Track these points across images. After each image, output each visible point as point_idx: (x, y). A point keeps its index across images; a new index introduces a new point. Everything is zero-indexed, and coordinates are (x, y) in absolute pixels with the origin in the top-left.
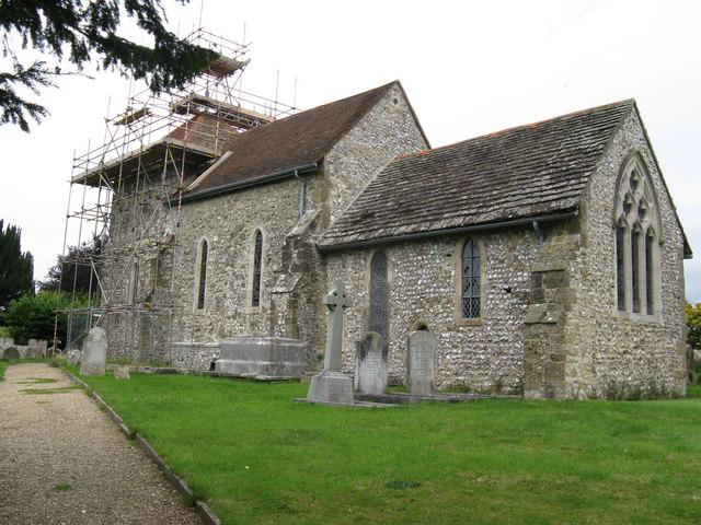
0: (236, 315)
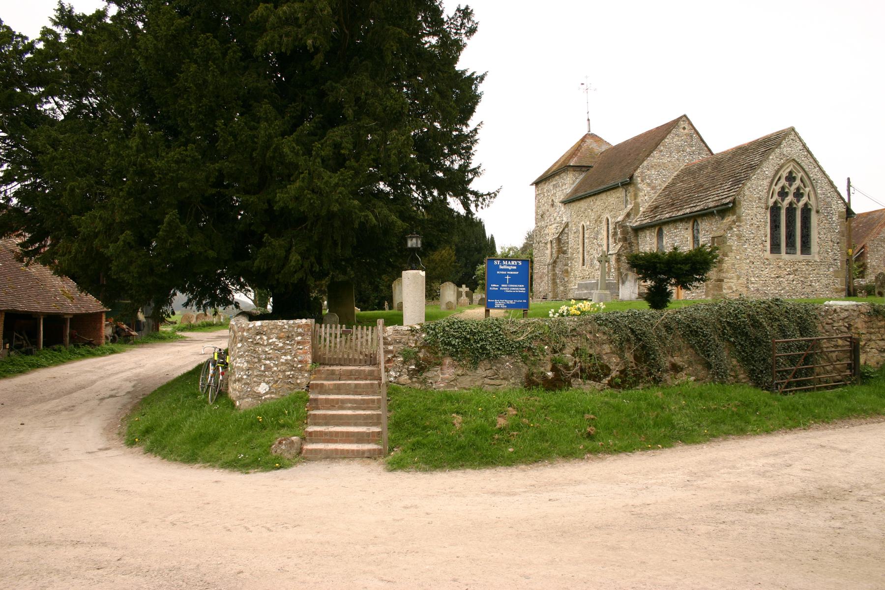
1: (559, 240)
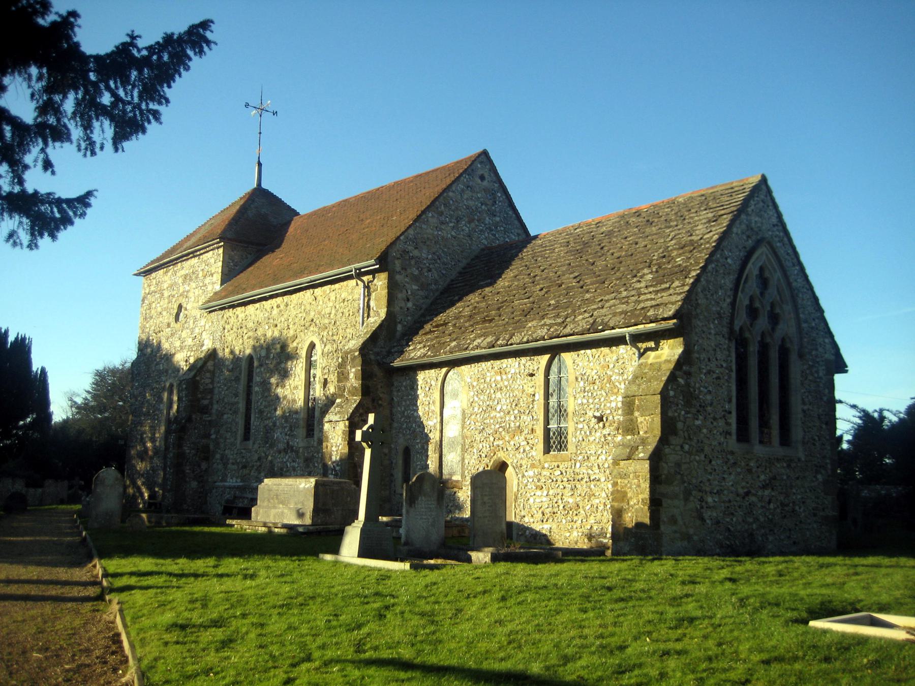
0: (289, 448)
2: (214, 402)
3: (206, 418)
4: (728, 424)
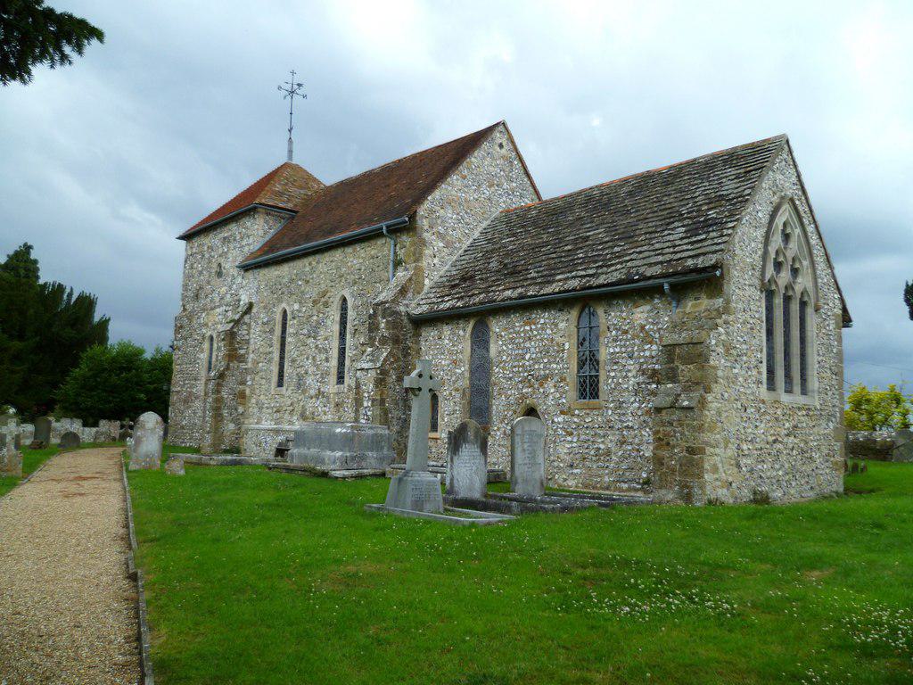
0: (320, 394)
1: (231, 336)
2: (251, 352)
3: (243, 366)
4: (759, 373)
